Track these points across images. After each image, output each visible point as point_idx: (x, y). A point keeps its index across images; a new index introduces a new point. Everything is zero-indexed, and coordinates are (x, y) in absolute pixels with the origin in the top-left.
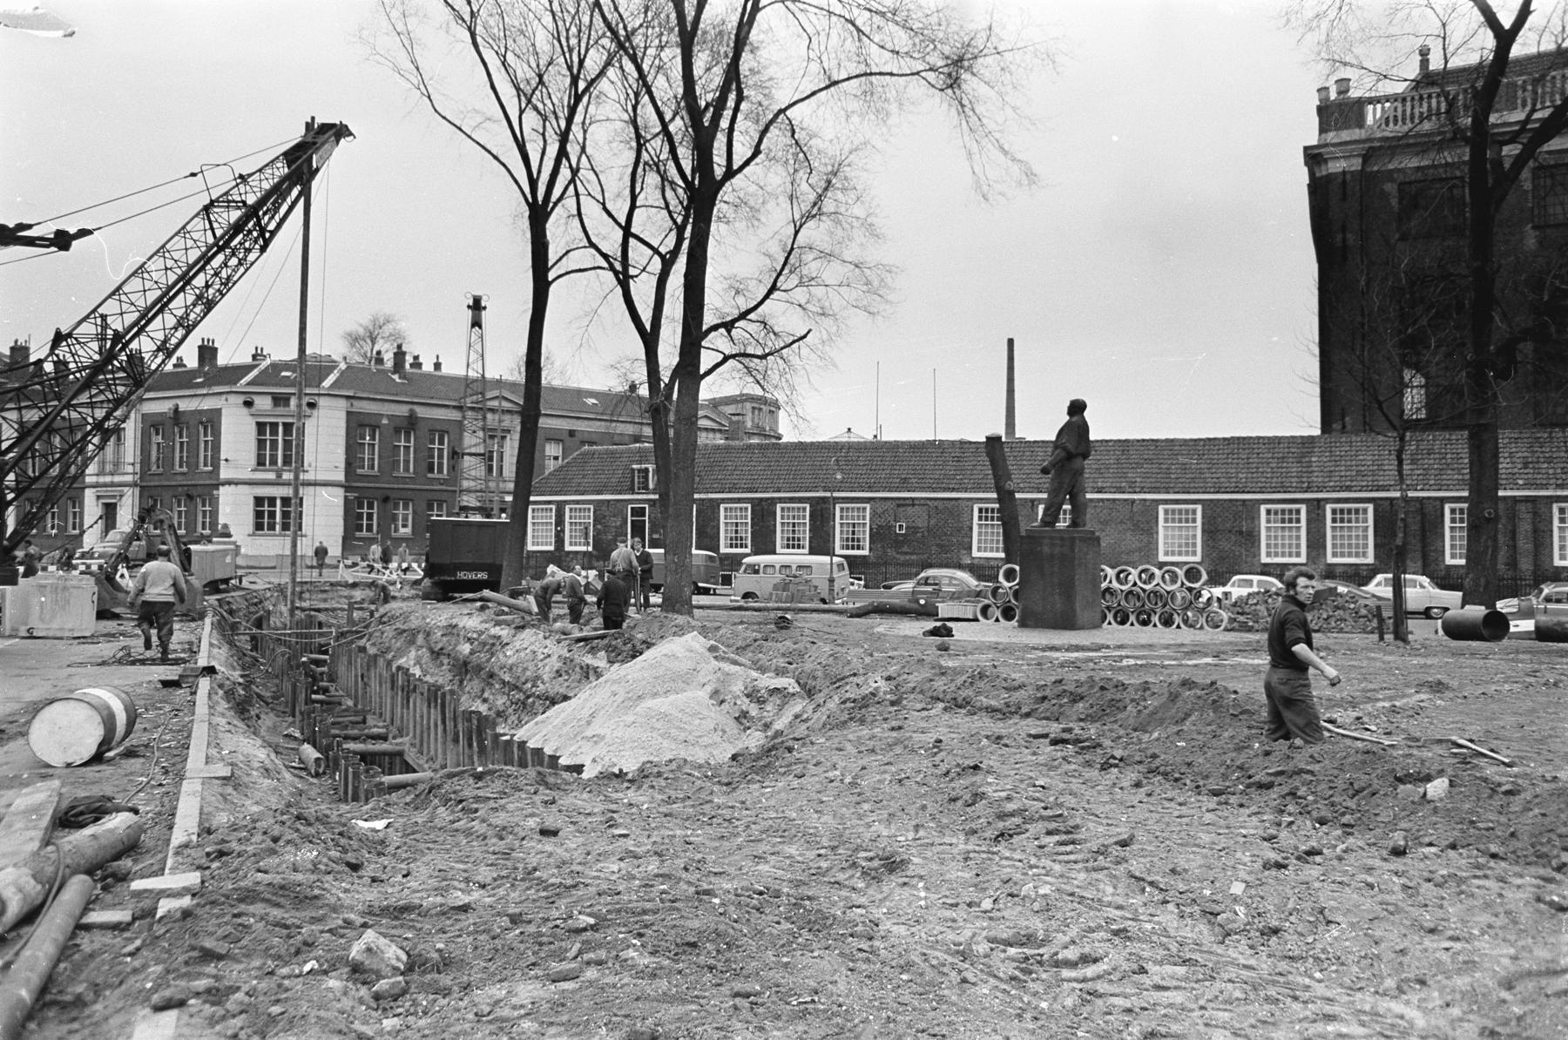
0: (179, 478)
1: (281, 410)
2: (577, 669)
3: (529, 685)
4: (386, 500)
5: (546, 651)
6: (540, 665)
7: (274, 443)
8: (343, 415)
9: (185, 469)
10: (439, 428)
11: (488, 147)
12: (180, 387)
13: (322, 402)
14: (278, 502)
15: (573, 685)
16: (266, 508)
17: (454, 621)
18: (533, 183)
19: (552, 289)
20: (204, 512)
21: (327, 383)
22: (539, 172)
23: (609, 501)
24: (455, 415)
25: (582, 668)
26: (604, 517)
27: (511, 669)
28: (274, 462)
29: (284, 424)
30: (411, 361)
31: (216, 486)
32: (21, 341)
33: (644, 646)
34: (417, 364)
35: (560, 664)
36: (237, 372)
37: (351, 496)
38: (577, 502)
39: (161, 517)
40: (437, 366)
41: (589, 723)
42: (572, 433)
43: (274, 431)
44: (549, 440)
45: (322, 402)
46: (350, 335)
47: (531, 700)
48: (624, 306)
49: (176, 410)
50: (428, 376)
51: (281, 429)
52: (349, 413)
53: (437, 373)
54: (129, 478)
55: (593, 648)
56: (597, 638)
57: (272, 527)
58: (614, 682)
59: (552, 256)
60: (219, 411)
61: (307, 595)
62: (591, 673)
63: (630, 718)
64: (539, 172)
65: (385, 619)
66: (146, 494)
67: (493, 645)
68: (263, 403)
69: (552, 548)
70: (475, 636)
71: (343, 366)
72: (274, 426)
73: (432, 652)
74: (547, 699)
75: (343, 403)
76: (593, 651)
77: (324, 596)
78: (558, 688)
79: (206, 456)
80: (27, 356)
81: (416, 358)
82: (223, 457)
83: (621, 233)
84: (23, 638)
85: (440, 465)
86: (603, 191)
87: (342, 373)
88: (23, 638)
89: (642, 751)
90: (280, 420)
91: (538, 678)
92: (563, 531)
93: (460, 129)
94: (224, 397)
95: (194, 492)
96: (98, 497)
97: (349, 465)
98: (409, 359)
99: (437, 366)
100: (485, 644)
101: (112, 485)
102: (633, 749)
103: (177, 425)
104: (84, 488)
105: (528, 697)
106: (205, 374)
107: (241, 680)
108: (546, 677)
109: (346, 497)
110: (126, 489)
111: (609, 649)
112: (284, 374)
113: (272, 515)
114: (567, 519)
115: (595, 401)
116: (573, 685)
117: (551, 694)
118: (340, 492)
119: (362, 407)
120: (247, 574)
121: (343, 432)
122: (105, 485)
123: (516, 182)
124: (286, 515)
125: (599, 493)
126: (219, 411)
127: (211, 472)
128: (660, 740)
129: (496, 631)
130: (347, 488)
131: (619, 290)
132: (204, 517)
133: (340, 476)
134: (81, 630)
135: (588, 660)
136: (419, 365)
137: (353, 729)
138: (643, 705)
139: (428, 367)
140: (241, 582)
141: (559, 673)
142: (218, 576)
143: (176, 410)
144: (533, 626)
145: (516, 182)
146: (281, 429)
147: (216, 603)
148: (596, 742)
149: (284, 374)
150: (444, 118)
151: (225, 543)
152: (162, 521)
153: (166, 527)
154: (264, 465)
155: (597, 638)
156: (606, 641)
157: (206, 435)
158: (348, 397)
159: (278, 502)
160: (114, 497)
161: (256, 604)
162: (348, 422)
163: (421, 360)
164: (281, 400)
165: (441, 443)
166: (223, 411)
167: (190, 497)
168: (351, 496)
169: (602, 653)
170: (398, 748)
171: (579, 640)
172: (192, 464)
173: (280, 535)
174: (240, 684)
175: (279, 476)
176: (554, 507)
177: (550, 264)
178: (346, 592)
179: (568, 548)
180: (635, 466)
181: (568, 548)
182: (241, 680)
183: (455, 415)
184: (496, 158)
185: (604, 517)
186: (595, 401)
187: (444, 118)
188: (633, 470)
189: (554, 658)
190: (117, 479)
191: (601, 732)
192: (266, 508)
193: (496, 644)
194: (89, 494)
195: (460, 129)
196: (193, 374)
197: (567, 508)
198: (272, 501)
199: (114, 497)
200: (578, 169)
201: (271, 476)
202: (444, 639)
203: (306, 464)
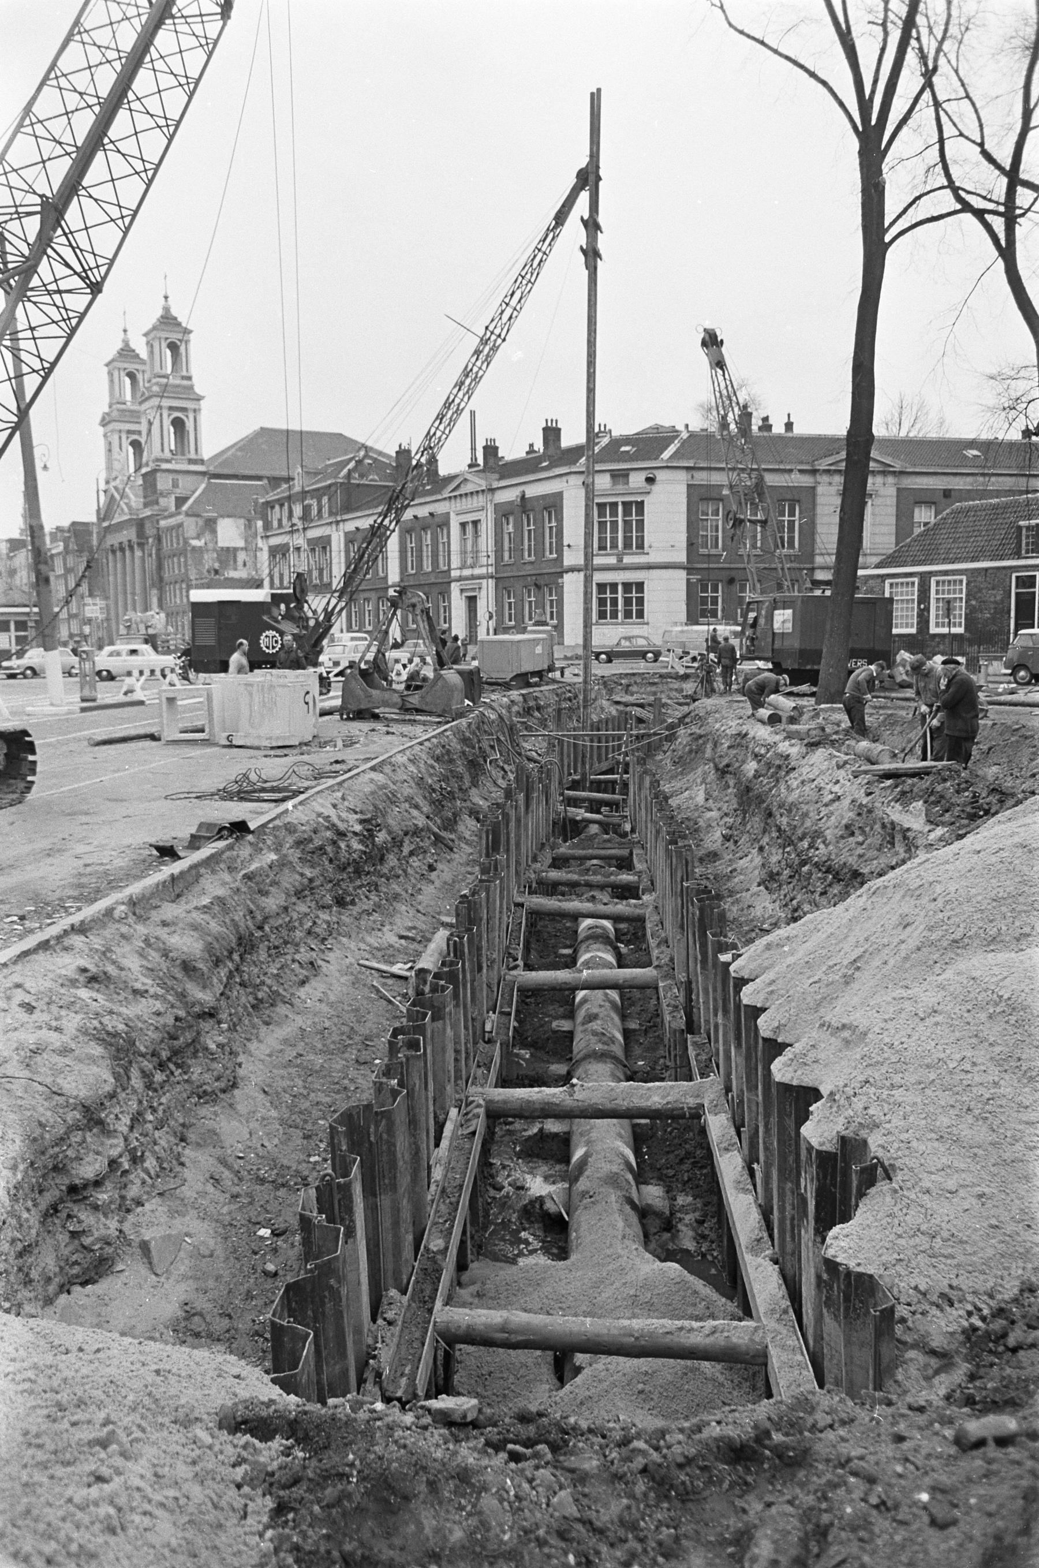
0: (528, 567)
1: (620, 488)
2: (877, 827)
3: (805, 844)
4: (731, 581)
5: (836, 788)
6: (824, 811)
7: (614, 524)
8: (684, 489)
9: (533, 558)
10: (789, 497)
11: (802, 62)
12: (527, 472)
13: (660, 475)
14: (620, 588)
15: (870, 854)
16: (608, 595)
17: (744, 729)
18: (865, 106)
19: (890, 254)
20: (552, 601)
21: (666, 455)
22: (873, 92)
23: (986, 570)
24: (806, 480)
25: (884, 826)
26: (980, 590)
27: (789, 811)
28: (614, 546)
29: (623, 503)
30: (760, 423)
31: (561, 574)
32: (405, 446)
33: (993, 799)
34: (766, 426)
35: (851, 814)
36: (576, 452)
37: (694, 578)
38: (946, 573)
39: (414, 600)
40: (789, 426)
41: (848, 979)
42: (947, 493)
43: (614, 513)
44: (919, 503)
45: (660, 475)
46: (702, 406)
47: (805, 869)
48: (1008, 289)
49: (523, 497)
50: (780, 437)
51: (620, 508)
52: (689, 486)
53: (790, 435)
54: (483, 571)
55: (903, 793)
56: (913, 775)
57: (614, 615)
58: (915, 893)
59: (892, 207)
60: (560, 495)
61: (634, 689)
62: (898, 837)
63: (929, 998)
64: (873, 92)
65: (687, 720)
66: (500, 586)
67: (779, 767)
68: (603, 482)
69: (913, 631)
70: (763, 751)
71: (685, 435)
72: (614, 505)
73: (717, 769)
74: (828, 871)
75: (682, 476)
76: (904, 798)
77: (654, 689)
78: (847, 855)
79: (551, 543)
80: (411, 459)
81: (766, 419)
82: (565, 543)
83: (1005, 181)
84: (225, 746)
85: (791, 540)
86: (981, 126)
87: (684, 443)
88: (225, 746)
89: (946, 1098)
90: (620, 499)
91: (818, 834)
92: (927, 609)
93: (762, 43)
94: (564, 479)
95: (541, 582)
96: (462, 591)
97: (691, 545)
98: (756, 424)
99: (789, 426)
100: (769, 765)
101: (473, 577)
102: (923, 1086)
103: (524, 512)
104: (449, 583)
105: (803, 863)
106: (550, 457)
107: (358, 828)
108: (829, 834)
109: (688, 580)
110: (484, 582)
111: (934, 800)
112: (623, 449)
113: (614, 602)
114: (933, 594)
115: (975, 452)
116: (870, 854)
117: (837, 862)
118: (682, 574)
119: (701, 478)
120: (569, 666)
121: (684, 508)
122: (467, 579)
123: (841, 104)
124: (628, 602)
125: (974, 559)
126: (560, 495)
127: (555, 560)
128: (994, 1074)
129: (784, 747)
130: (690, 570)
131: (1000, 264)
132: (552, 607)
133: (682, 557)
134: (284, 738)
135: (896, 814)
136: (769, 428)
137: (594, 874)
138: (962, 965)
139: (778, 429)
140: (562, 675)
141: (849, 830)
142: (527, 667)
143: (523, 497)
144: (833, 743)
145: (841, 104)
146: (620, 508)
147: (521, 699)
148: (847, 1042)
149: (623, 449)
150: (741, 32)
151: (539, 632)
152: (414, 606)
153: (418, 612)
154: (605, 548)
155: (913, 775)
156: (926, 783)
157: (550, 521)
158: (688, 468)
159: (620, 588)
160: (473, 589)
161: (570, 699)
162: (689, 496)
163: (771, 422)
164: (619, 476)
165: (792, 514)
166: (565, 496)
167: (538, 587)
168: (694, 578)
169: (919, 804)
170: (638, 911)
171: (887, 775)
172: (540, 552)
173: (622, 623)
174: (355, 834)
175: (620, 560)
176: (916, 580)
177: (886, 224)
178: (676, 685)
179: (933, 630)
180: (1022, 523)
181: (933, 630)
182: (358, 828)
183: (806, 480)
184: (813, 75)
185: (980, 590)
186: (975, 452)
187: (741, 32)
188: (1020, 528)
189: (846, 802)
190: (477, 571)
191: (859, 1018)
192: (634, 594)
193: (782, 767)
194: (455, 587)
195: (762, 43)
196: (540, 459)
197: (933, 580)
198: (614, 586)
199: (473, 589)
200: (935, 69)
201: (612, 560)
202: (733, 752)
203: (646, 545)
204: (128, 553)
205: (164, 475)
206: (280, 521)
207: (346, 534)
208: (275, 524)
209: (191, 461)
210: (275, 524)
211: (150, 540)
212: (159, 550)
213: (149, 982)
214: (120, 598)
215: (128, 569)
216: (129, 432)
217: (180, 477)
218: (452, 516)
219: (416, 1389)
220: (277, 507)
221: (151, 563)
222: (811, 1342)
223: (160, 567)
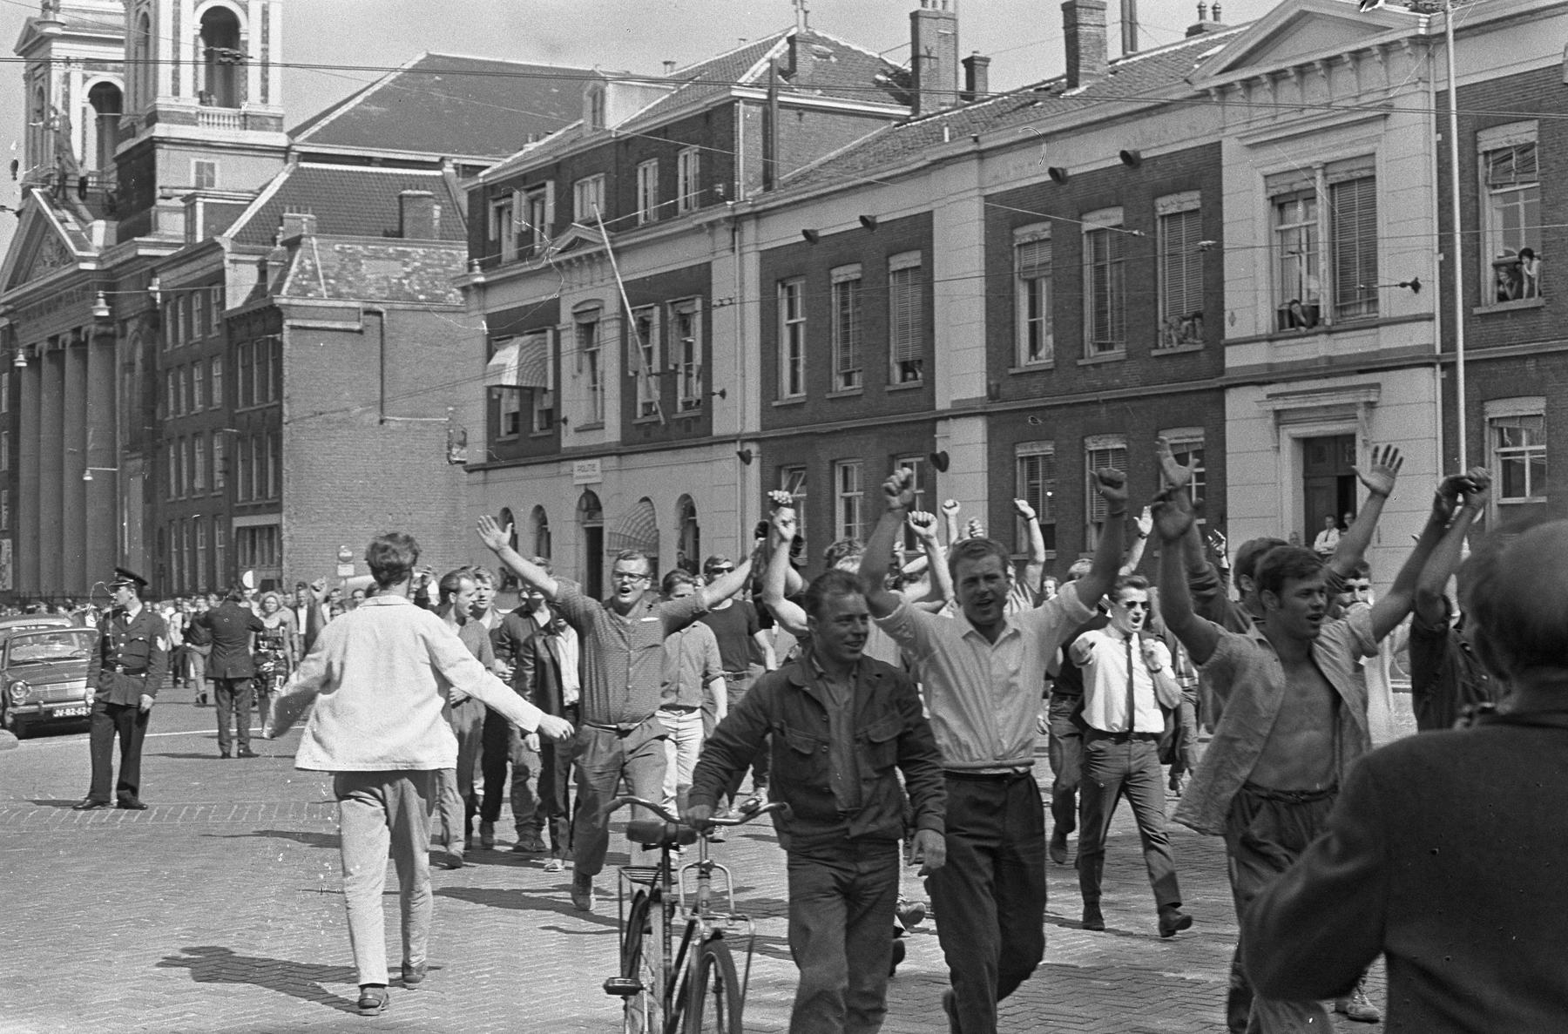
82: (716, 389)
160: (1347, 413)
194: (1242, 408)
204: (70, 361)
205: (177, 154)
206: (526, 237)
207: (766, 257)
208: (509, 250)
209: (247, 121)
210: (509, 250)
211: (131, 327)
212: (150, 354)
213: (159, 496)
214: (47, 482)
215: (71, 403)
216: (90, 63)
217: (218, 161)
218: (1231, 150)
219: (63, 148)
220: (519, 199)
221: (130, 388)
222: (526, 894)
223: (153, 395)
